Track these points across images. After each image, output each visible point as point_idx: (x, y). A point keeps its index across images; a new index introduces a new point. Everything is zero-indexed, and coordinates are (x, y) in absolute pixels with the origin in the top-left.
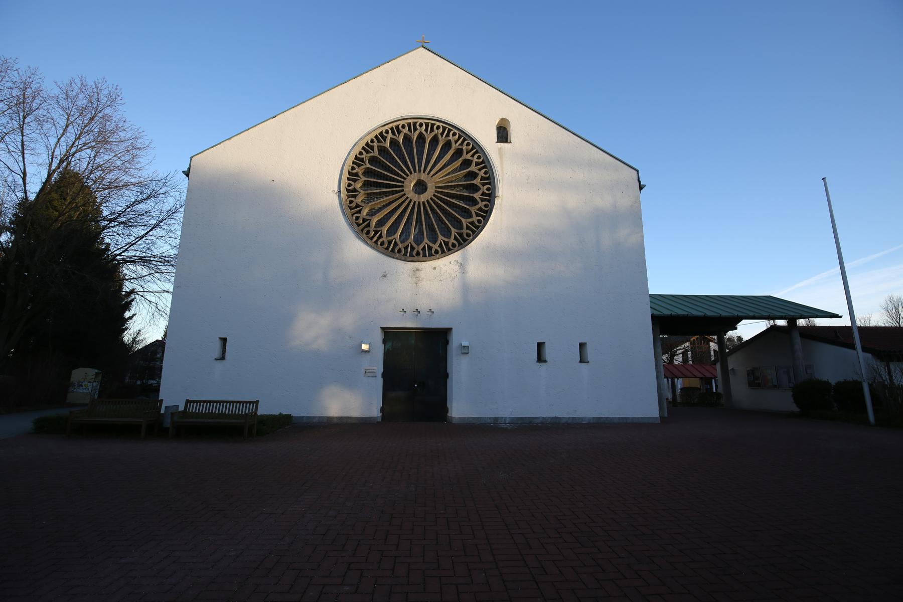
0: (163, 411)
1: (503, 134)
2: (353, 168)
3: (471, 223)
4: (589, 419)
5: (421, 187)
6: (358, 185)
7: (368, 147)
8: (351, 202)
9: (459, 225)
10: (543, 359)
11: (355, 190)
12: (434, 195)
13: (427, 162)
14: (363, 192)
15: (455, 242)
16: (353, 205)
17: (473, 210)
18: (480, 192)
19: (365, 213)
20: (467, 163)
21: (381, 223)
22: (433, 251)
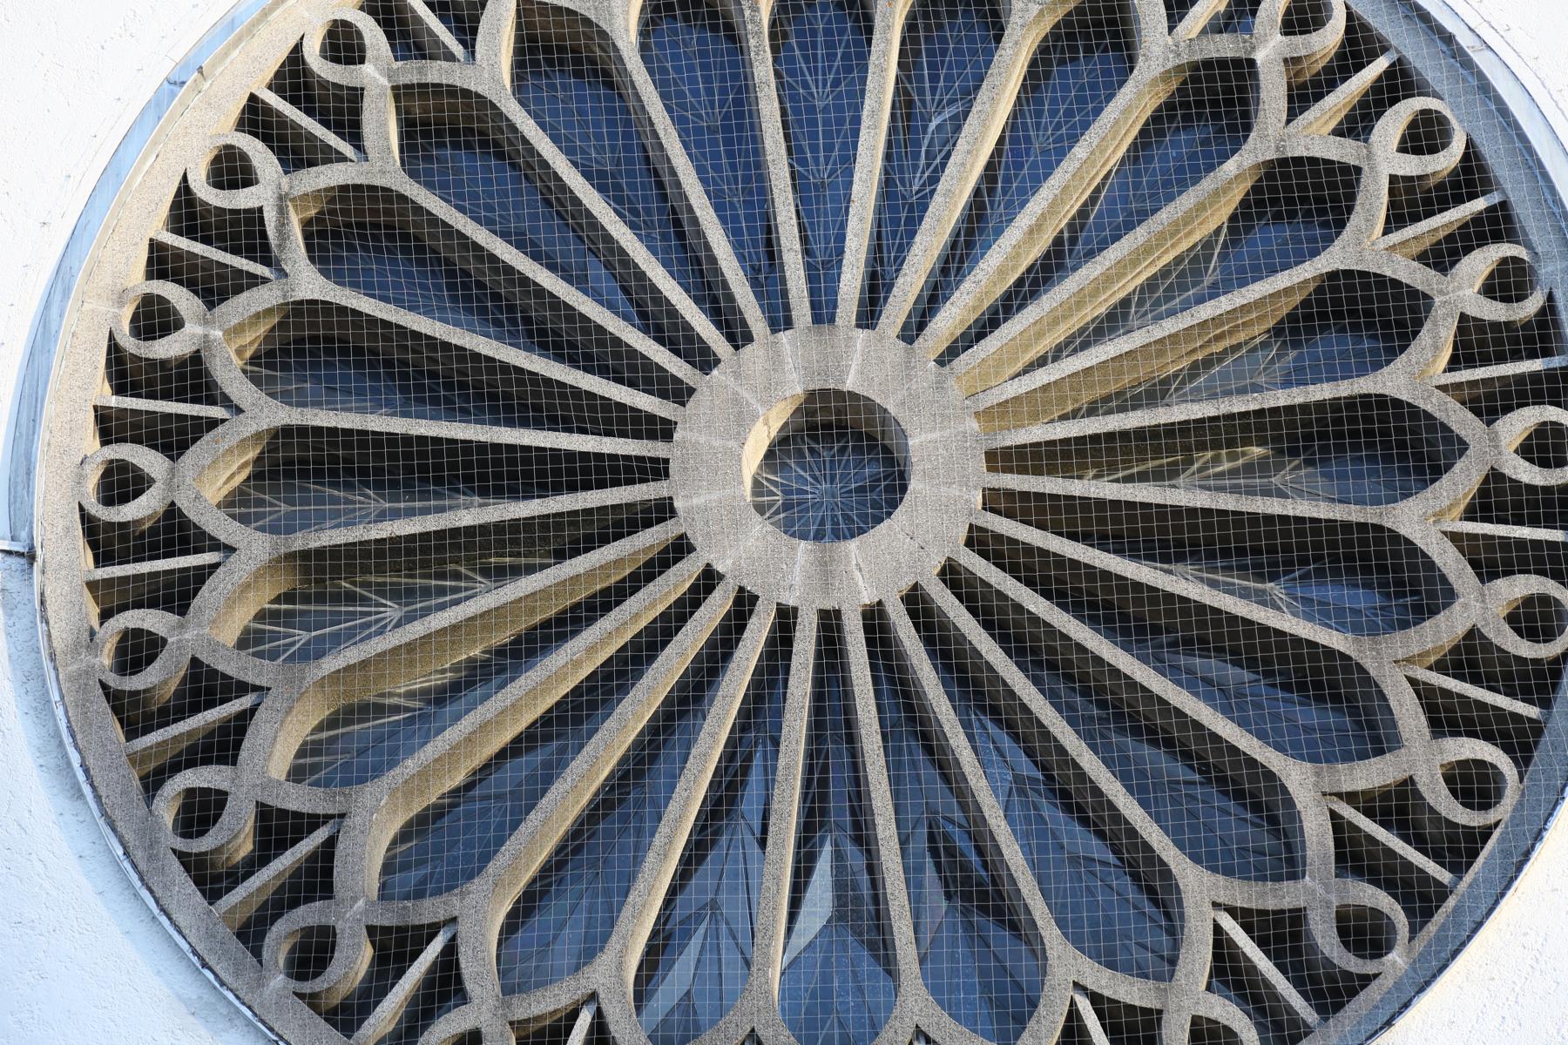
2: (154, 319)
3: (1366, 802)
5: (842, 457)
6: (205, 482)
7: (206, 240)
8: (137, 651)
9: (1251, 817)
11: (175, 532)
12: (978, 540)
13: (900, 215)
14: (255, 548)
16: (235, 834)
17: (1397, 663)
18: (1462, 481)
19: (280, 761)
20: (1306, 198)
21: (444, 842)
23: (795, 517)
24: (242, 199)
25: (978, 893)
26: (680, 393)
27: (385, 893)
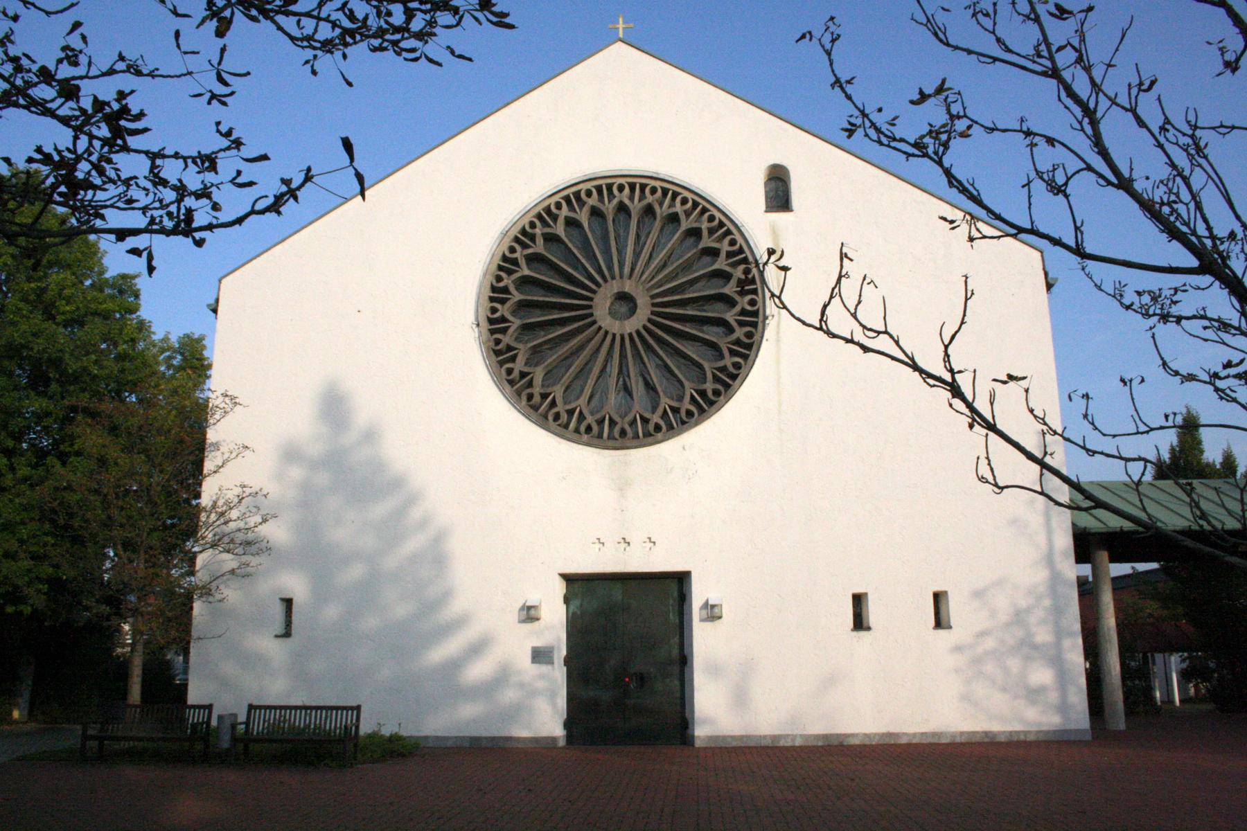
0: (214, 723)
1: (778, 191)
4: (953, 735)
10: (944, 622)
15: (662, 423)
22: (651, 427)
23: (613, 313)
24: (514, 256)
25: (649, 386)
26: (594, 292)
27: (543, 386)
